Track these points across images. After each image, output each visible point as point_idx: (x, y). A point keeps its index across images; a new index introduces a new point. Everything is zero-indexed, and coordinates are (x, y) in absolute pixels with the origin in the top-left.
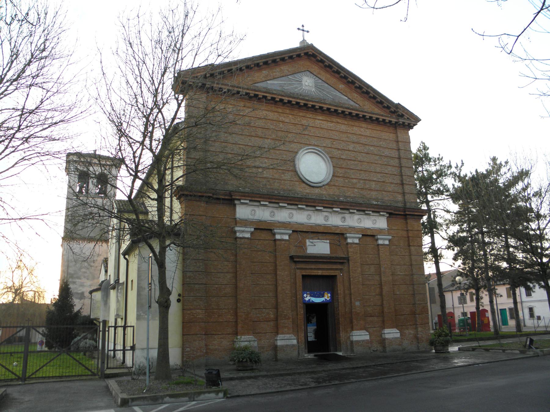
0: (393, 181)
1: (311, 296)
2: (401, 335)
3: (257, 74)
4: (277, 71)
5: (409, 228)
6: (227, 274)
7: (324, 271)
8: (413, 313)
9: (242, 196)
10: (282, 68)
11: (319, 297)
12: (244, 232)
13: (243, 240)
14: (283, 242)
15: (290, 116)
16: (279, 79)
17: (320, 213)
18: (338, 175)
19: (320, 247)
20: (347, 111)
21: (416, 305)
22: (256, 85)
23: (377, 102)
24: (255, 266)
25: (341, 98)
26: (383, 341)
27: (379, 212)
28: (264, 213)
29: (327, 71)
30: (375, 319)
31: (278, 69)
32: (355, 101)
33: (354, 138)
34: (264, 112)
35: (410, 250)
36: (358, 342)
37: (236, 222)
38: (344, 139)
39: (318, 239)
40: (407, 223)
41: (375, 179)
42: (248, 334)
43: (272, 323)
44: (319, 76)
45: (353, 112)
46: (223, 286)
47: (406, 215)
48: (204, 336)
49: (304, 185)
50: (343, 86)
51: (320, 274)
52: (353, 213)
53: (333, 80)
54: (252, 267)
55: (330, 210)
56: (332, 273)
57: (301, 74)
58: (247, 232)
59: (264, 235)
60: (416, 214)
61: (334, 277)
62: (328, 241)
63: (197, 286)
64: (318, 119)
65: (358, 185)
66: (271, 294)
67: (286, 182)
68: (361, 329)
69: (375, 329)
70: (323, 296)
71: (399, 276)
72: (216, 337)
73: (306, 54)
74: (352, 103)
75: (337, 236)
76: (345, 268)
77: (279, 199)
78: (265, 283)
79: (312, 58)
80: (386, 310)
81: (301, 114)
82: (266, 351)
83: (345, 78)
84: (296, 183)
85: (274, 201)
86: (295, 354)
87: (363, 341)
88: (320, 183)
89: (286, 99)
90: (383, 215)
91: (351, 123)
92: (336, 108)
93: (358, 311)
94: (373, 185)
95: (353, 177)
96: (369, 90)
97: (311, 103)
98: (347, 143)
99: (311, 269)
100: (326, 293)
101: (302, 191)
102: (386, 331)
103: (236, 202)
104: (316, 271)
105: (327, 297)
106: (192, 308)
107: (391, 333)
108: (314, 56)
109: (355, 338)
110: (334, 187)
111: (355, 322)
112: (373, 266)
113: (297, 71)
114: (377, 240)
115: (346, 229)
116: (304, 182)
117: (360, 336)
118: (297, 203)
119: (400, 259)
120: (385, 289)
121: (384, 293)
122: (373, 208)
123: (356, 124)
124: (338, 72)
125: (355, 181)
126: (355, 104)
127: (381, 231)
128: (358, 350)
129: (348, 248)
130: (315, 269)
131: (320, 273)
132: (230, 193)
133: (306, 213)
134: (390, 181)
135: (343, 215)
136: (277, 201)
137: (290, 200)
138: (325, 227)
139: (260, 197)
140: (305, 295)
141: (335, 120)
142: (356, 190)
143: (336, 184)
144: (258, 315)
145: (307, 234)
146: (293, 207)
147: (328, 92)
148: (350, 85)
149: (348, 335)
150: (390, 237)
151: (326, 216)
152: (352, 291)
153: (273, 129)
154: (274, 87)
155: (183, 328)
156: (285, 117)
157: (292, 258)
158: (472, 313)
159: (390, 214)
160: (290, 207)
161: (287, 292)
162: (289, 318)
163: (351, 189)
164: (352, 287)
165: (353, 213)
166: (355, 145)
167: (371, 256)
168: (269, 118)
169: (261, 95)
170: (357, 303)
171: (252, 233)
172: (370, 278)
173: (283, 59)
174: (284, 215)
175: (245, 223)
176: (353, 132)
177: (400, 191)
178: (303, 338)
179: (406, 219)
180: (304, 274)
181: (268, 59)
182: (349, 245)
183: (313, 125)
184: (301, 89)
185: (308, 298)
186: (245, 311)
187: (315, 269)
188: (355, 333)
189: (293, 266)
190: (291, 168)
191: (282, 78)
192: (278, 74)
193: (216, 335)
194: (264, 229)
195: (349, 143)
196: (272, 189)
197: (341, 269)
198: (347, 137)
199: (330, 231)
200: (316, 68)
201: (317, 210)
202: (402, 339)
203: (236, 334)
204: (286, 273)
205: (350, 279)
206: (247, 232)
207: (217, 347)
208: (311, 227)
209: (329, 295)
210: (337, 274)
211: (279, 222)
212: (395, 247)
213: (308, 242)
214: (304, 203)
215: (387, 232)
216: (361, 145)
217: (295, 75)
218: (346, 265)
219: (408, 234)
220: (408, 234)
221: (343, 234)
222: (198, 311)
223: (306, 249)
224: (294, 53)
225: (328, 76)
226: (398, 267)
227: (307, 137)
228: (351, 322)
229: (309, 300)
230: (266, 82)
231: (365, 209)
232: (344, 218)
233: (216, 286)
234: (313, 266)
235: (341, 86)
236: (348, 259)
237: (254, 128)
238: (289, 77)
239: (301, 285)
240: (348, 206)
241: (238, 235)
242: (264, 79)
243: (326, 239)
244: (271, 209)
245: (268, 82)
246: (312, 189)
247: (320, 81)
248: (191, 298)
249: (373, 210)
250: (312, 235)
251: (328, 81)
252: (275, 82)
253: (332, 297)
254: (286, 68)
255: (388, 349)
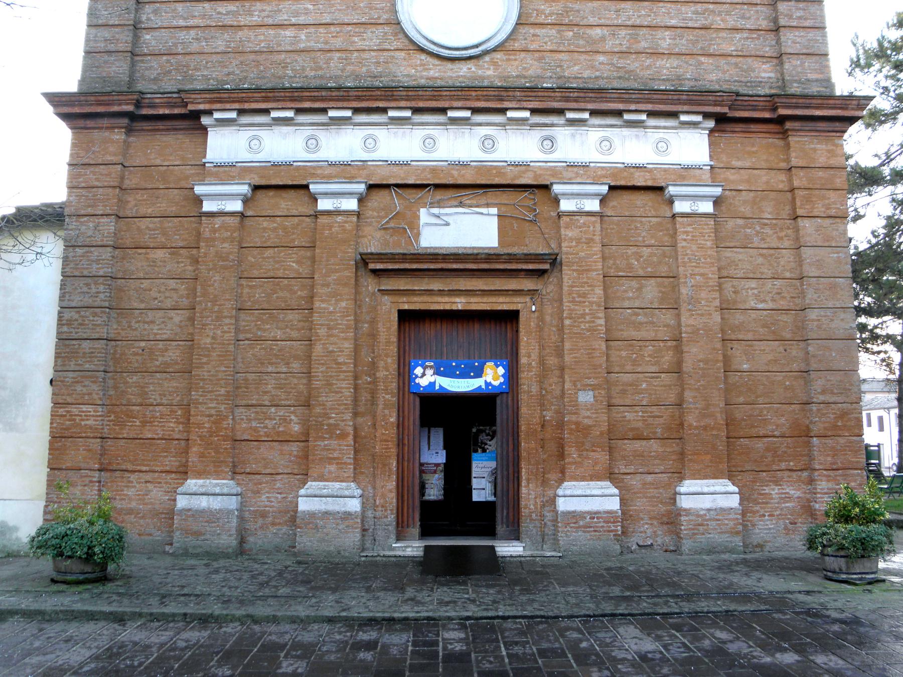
0: (740, 24)
1: (437, 373)
2: (742, 500)
5: (794, 162)
6: (172, 313)
7: (473, 300)
8: (803, 433)
9: (212, 101)
11: (464, 375)
12: (223, 199)
13: (218, 221)
14: (339, 219)
17: (466, 130)
18: (542, 19)
19: (471, 229)
21: (814, 408)
24: (251, 287)
26: (672, 518)
27: (674, 115)
28: (282, 144)
30: (654, 446)
35: (797, 230)
36: (574, 516)
37: (204, 172)
39: (461, 205)
40: (788, 146)
41: (673, 22)
42: (218, 475)
43: (294, 448)
46: (161, 345)
47: (781, 120)
48: (97, 474)
49: (423, 57)
51: (460, 307)
52: (582, 122)
54: (246, 290)
55: (440, 118)
56: (502, 304)
58: (350, 194)
59: (286, 203)
60: (818, 113)
61: (511, 317)
62: (494, 211)
63: (86, 344)
65: (609, 45)
66: (296, 366)
67: (366, 55)
68: (599, 478)
69: (649, 478)
70: (479, 374)
71: (753, 314)
72: (133, 477)
75: (523, 192)
76: (547, 287)
77: (323, 99)
78: (279, 334)
80: (691, 419)
82: (273, 524)
84: (398, 54)
85: (307, 105)
86: (352, 539)
87: (594, 515)
88: (477, 46)
90: (694, 125)
93: (586, 421)
94: (665, 41)
95: (592, 20)
99: (430, 292)
100: (490, 364)
101: (410, 71)
102: (688, 486)
103: (205, 120)
104: (446, 299)
105: (493, 376)
106: (69, 400)
107: (708, 496)
109: (563, 505)
110: (523, 55)
111: (572, 453)
112: (652, 281)
114: (671, 202)
115: (554, 172)
116: (422, 50)
117: (587, 497)
118: (381, 104)
119: (760, 260)
120: (694, 353)
121: (687, 366)
122: (649, 101)
125: (598, 31)
127: (685, 173)
128: (575, 540)
129: (559, 227)
130: (441, 292)
131: (459, 303)
132: (181, 96)
133: (419, 133)
134: (731, 23)
135: (547, 132)
136: (317, 105)
137: (359, 98)
138: (482, 167)
139: (266, 99)
140: (419, 371)
142: (601, 58)
143: (532, 47)
144: (254, 424)
145: (420, 193)
146: (662, 122)
149: (550, 493)
150: (718, 191)
151: (487, 137)
152: (567, 358)
155: (52, 449)
157: (364, 260)
158: (476, 451)
159: (721, 119)
160: (362, 118)
161: (341, 360)
162: (343, 436)
163: (583, 57)
164: (567, 345)
165: (582, 122)
167: (646, 251)
170: (586, 397)
171: (246, 201)
172: (640, 318)
174: (348, 143)
175: (227, 172)
177: (768, 51)
178: (393, 495)
179: (784, 134)
180: (406, 307)
182: (565, 219)
185: (426, 378)
186: (213, 412)
187: (441, 292)
188: (569, 487)
189: (371, 285)
190: (385, 16)
193: (134, 471)
194: (282, 186)
196: (322, 77)
197: (532, 292)
199: (497, 181)
201: (454, 121)
202: (744, 514)
203: (184, 473)
204: (343, 304)
205: (561, 319)
206: (350, 194)
207: (133, 504)
208: (434, 170)
209: (501, 371)
210: (519, 307)
211: (332, 164)
212: (740, 222)
213: (424, 216)
214: (403, 104)
215: (707, 176)
218: (553, 278)
219: (790, 181)
220: (790, 181)
221: (546, 188)
222: (84, 408)
223: (418, 235)
226: (753, 284)
228: (562, 456)
229: (432, 384)
231: (621, 106)
232: (551, 139)
233: (143, 344)
234: (436, 285)
236: (554, 261)
239: (394, 339)
240: (550, 103)
241: (566, 205)
243: (488, 205)
244: (308, 131)
246: (449, 65)
248: (71, 374)
249: (649, 107)
250: (440, 195)
253: (512, 375)
255: (687, 545)
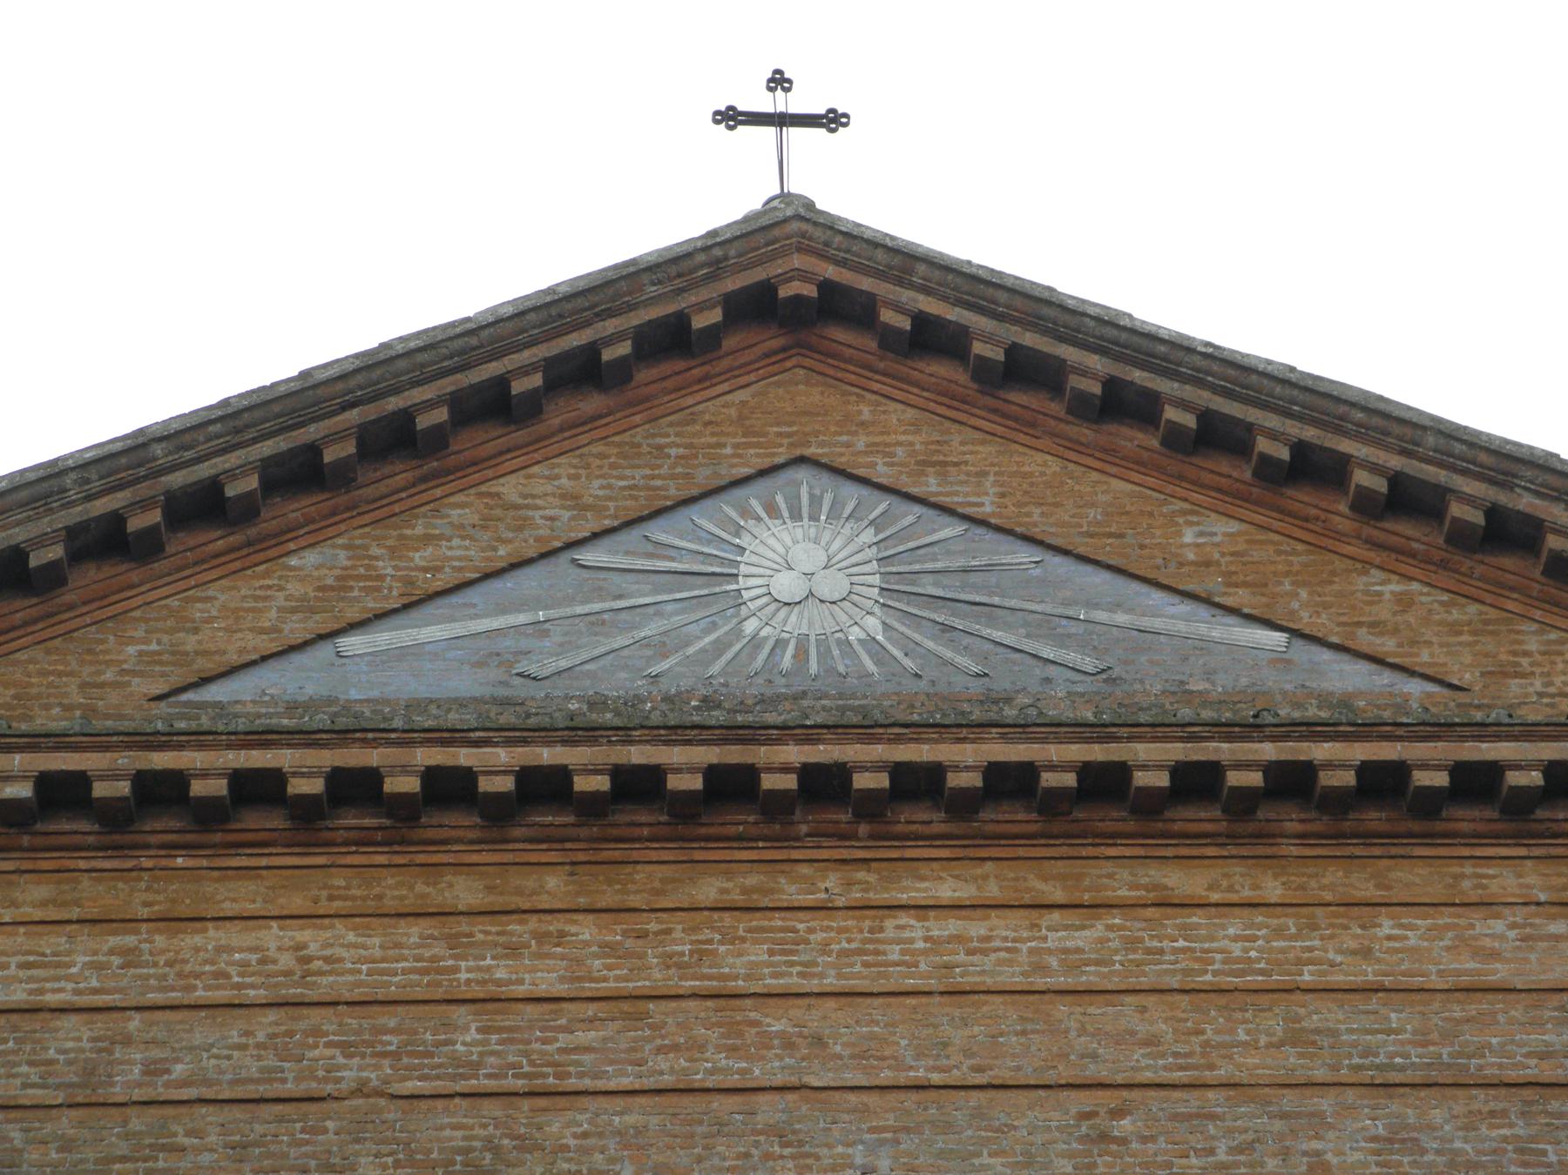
3: (223, 596)
4: (451, 529)
10: (509, 488)
15: (585, 930)
16: (473, 595)
20: (1245, 762)
22: (216, 692)
23: (1275, 476)
25: (1205, 646)
29: (1027, 424)
31: (462, 510)
32: (1387, 645)
33: (1396, 1035)
34: (272, 936)
38: (1252, 1065)
44: (931, 485)
45: (1320, 751)
50: (1223, 527)
53: (1097, 495)
57: (726, 506)
64: (920, 909)
73: (757, 307)
74: (1347, 678)
79: (840, 335)
81: (709, 889)
83: (1216, 436)
89: (496, 767)
91: (1333, 879)
92: (1098, 753)
96: (1524, 502)
97: (794, 754)
98: (1288, 1100)
108: (838, 306)
113: (674, 492)
123: (1414, 876)
124: (1120, 405)
126: (1384, 679)
141: (1121, 878)
147: (1046, 626)
148: (1302, 498)
153: (361, 1090)
154: (404, 685)
156: (513, 950)
166: (1405, 1109)
168: (325, 986)
169: (306, 769)
173: (494, 406)
176: (1369, 973)
181: (312, 432)
183: (858, 975)
184: (720, 647)
191: (507, 584)
192: (462, 554)
195: (1325, 1103)
198: (1295, 1038)
200: (897, 414)
216: (1482, 1100)
217: (658, 531)
224: (610, 326)
225: (1041, 465)
227: (769, 1109)
230: (324, 651)
235: (1205, 533)
237: (138, 1121)
238: (588, 556)
242: (296, 628)
245: (353, 643)
247: (951, 530)
251: (1036, 519)
252: (428, 631)
254: (543, 487)
